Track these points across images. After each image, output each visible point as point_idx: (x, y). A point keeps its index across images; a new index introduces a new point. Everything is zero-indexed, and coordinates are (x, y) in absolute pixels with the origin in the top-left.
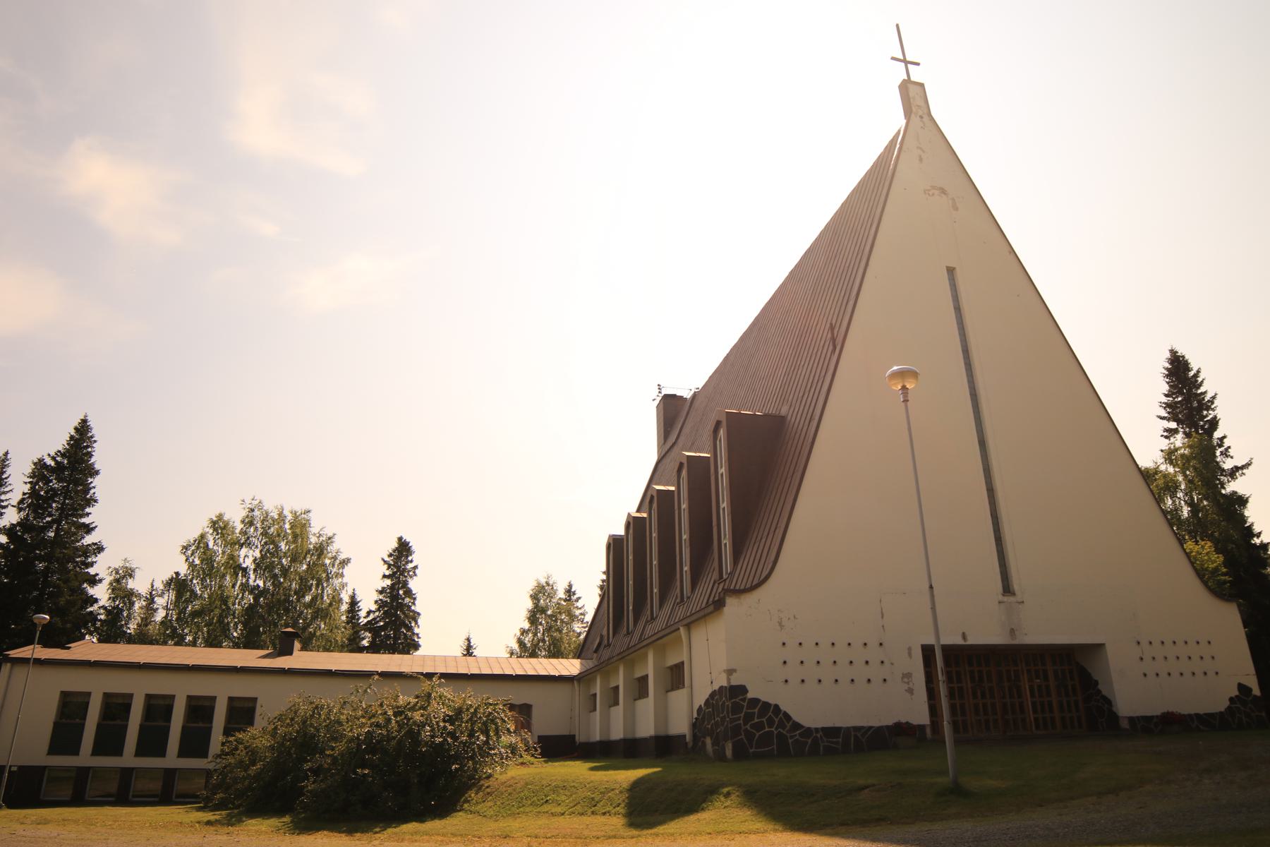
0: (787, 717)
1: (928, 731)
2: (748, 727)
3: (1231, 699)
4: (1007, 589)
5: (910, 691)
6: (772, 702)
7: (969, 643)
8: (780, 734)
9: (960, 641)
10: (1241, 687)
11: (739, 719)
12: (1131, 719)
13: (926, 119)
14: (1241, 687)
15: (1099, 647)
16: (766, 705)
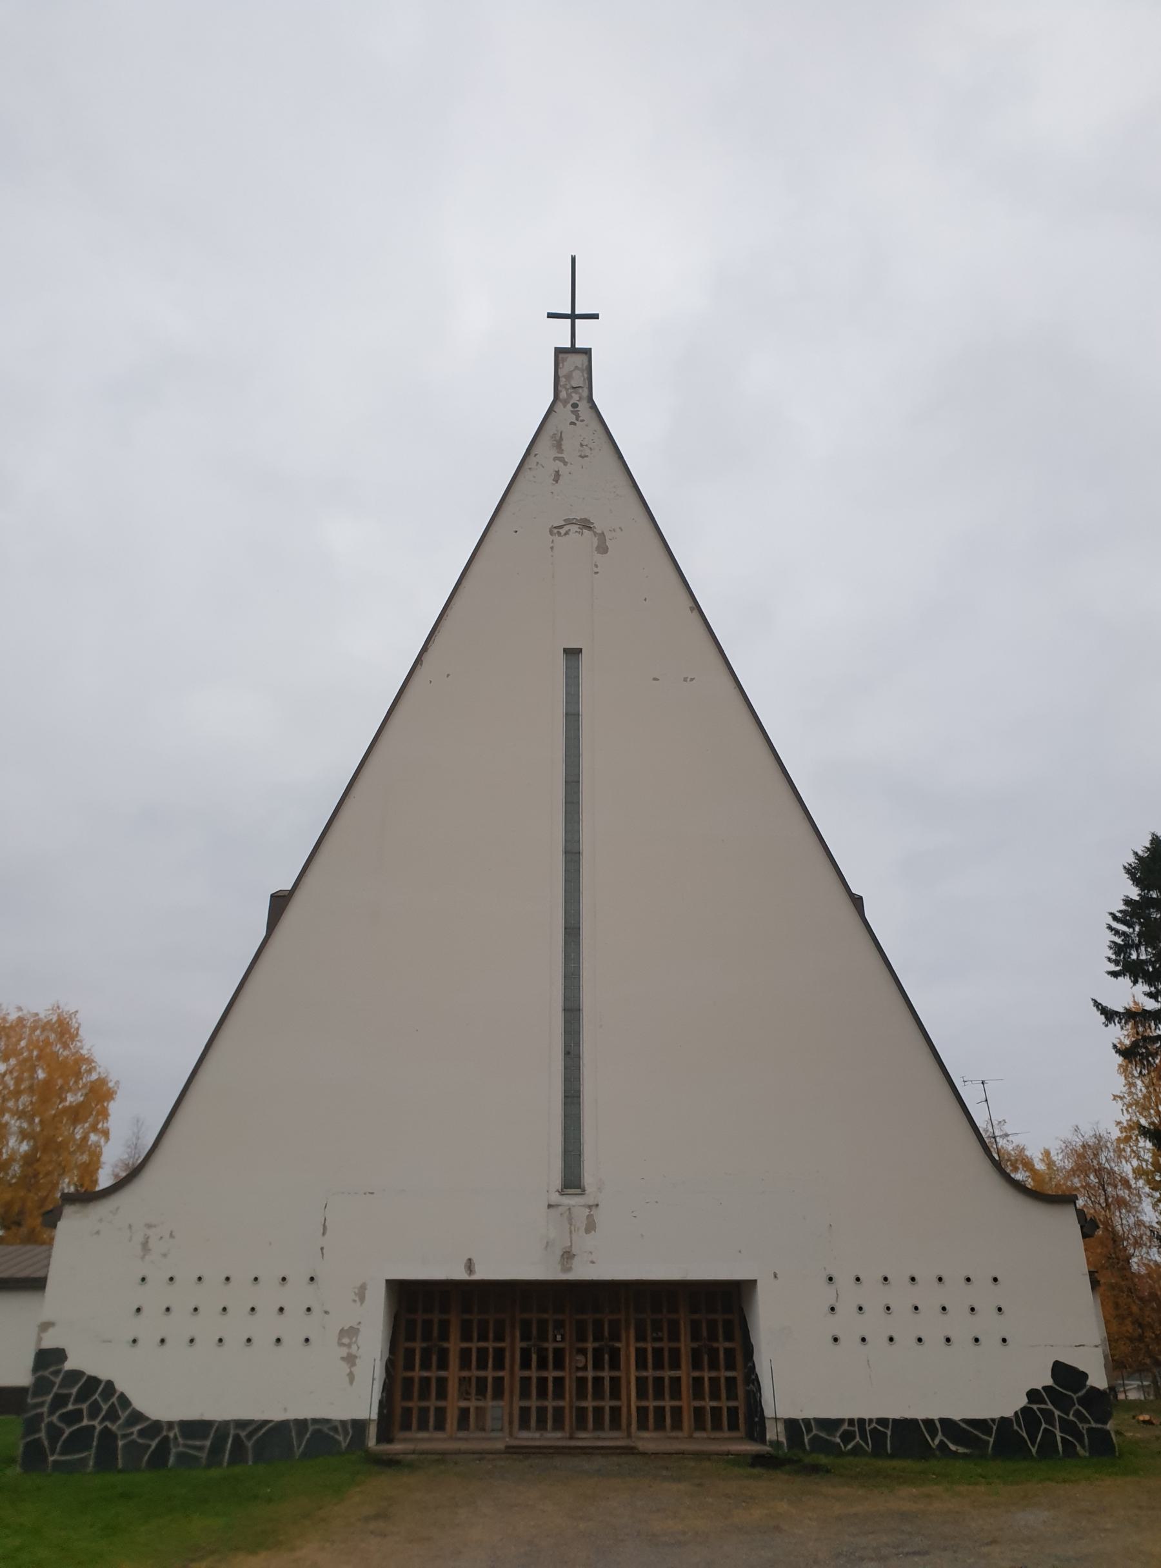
0: (124, 1401)
1: (373, 1431)
2: (55, 1418)
3: (1033, 1395)
4: (572, 1181)
5: (350, 1359)
6: (104, 1376)
7: (478, 1276)
8: (106, 1432)
9: (460, 1274)
10: (1061, 1370)
11: (42, 1404)
12: (792, 1425)
13: (583, 407)
14: (1061, 1370)
15: (753, 1283)
16: (93, 1381)
